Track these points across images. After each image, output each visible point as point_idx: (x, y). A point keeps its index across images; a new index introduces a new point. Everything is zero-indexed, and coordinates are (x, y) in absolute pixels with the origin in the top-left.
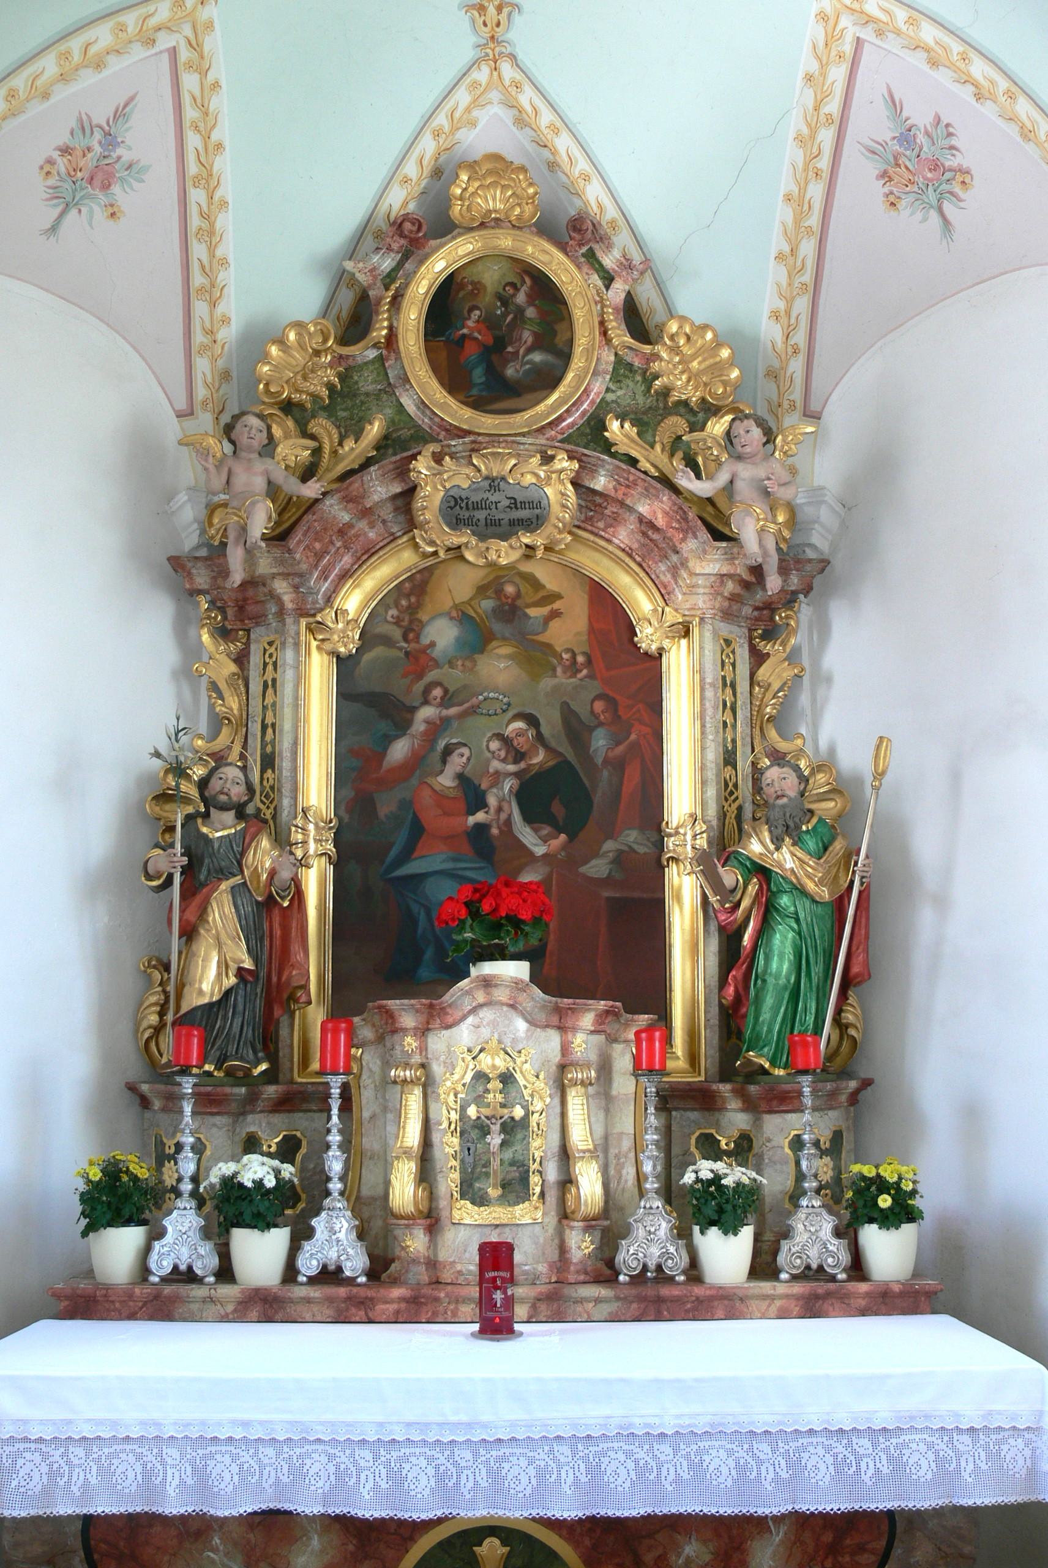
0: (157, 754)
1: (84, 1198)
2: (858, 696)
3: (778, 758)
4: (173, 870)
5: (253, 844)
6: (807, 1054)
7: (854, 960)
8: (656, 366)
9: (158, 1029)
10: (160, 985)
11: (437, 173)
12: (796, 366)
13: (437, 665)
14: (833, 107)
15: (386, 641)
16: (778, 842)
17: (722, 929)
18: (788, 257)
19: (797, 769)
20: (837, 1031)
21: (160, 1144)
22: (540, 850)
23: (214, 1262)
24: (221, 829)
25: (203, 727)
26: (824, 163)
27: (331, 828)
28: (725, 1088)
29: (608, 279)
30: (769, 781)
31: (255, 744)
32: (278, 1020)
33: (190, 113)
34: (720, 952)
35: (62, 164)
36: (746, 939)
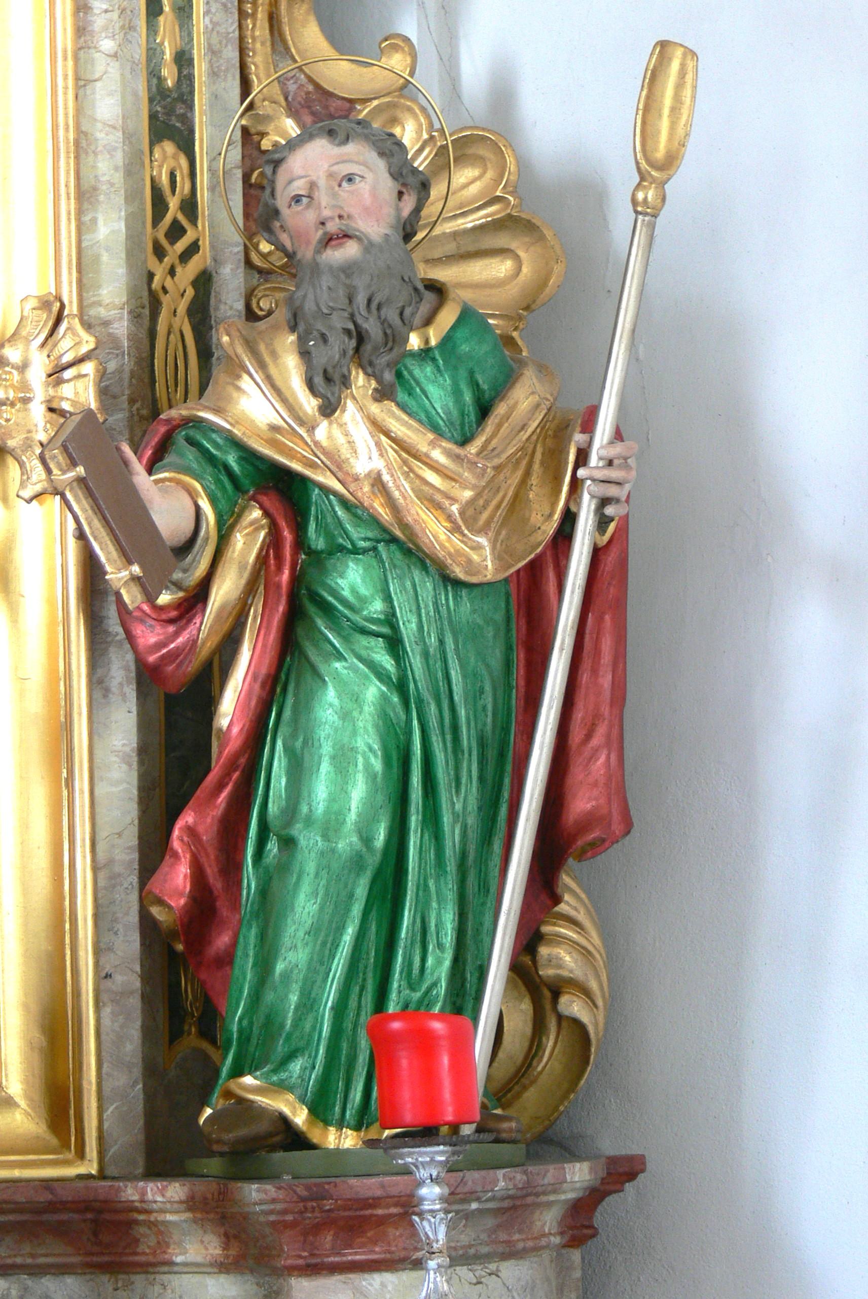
3: (327, 113)
6: (429, 1076)
7: (577, 774)
16: (329, 388)
17: (148, 676)
19: (390, 148)
20: (526, 1005)
28: (165, 1196)
30: (299, 187)
34: (143, 750)
36: (230, 707)
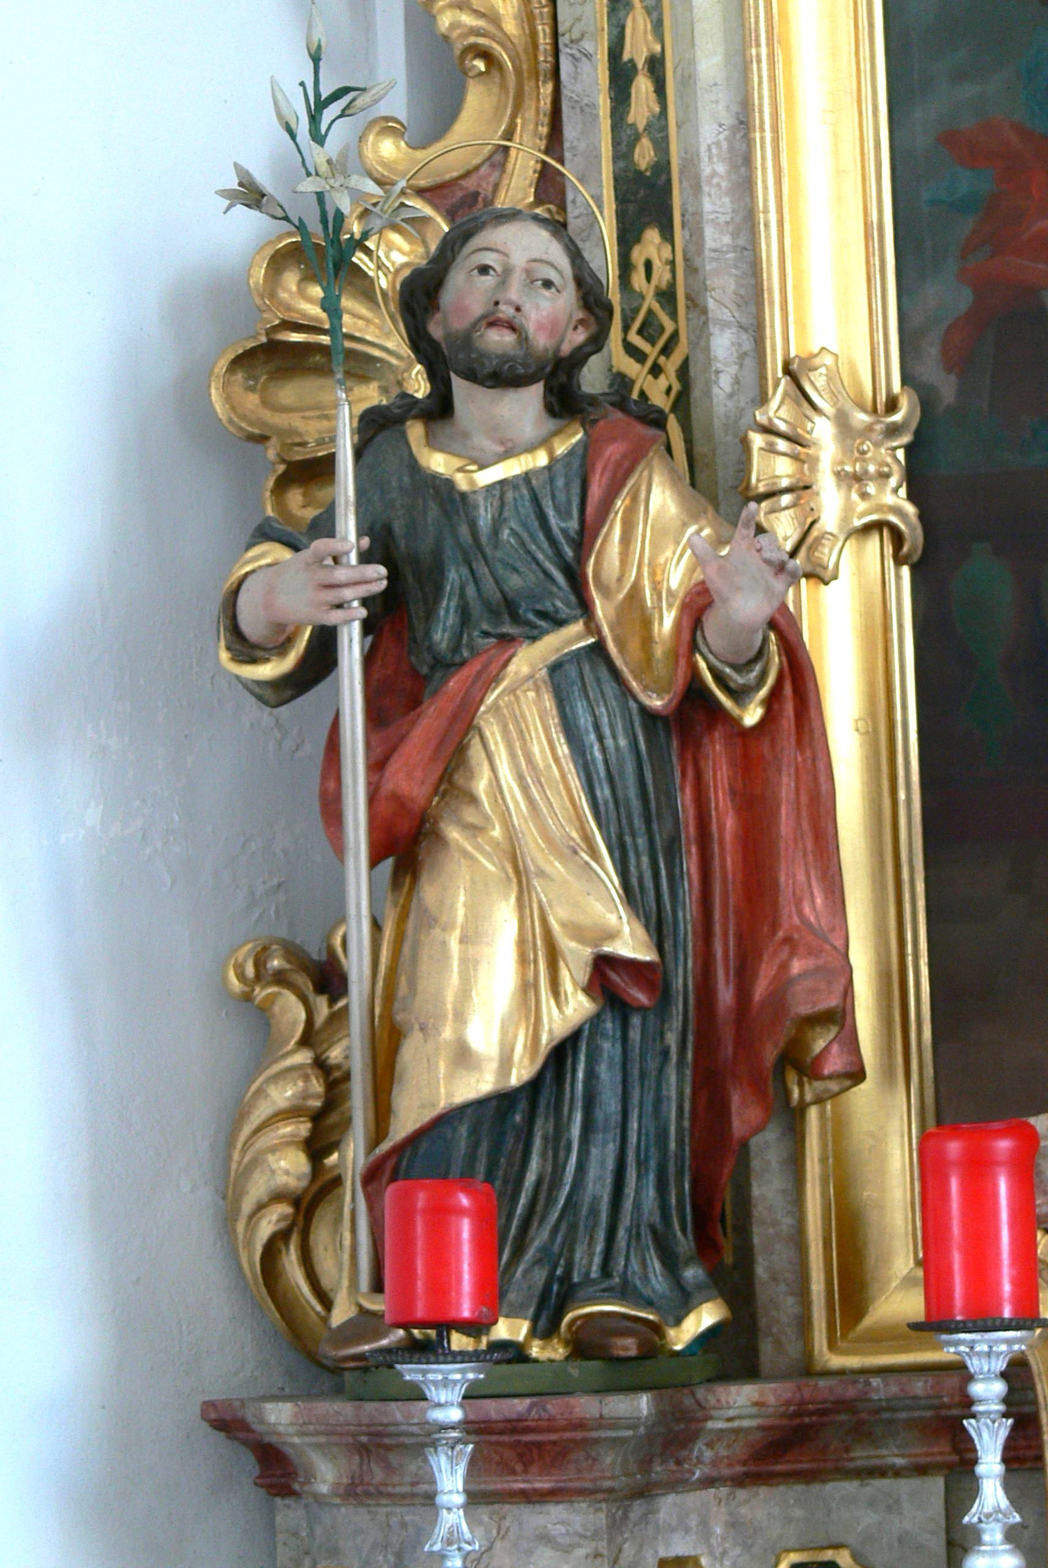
0: (251, 194)
4: (334, 617)
5: (620, 504)
9: (309, 1203)
10: (307, 1040)
24: (500, 451)
27: (893, 431)
31: (592, 140)
32: (744, 1144)
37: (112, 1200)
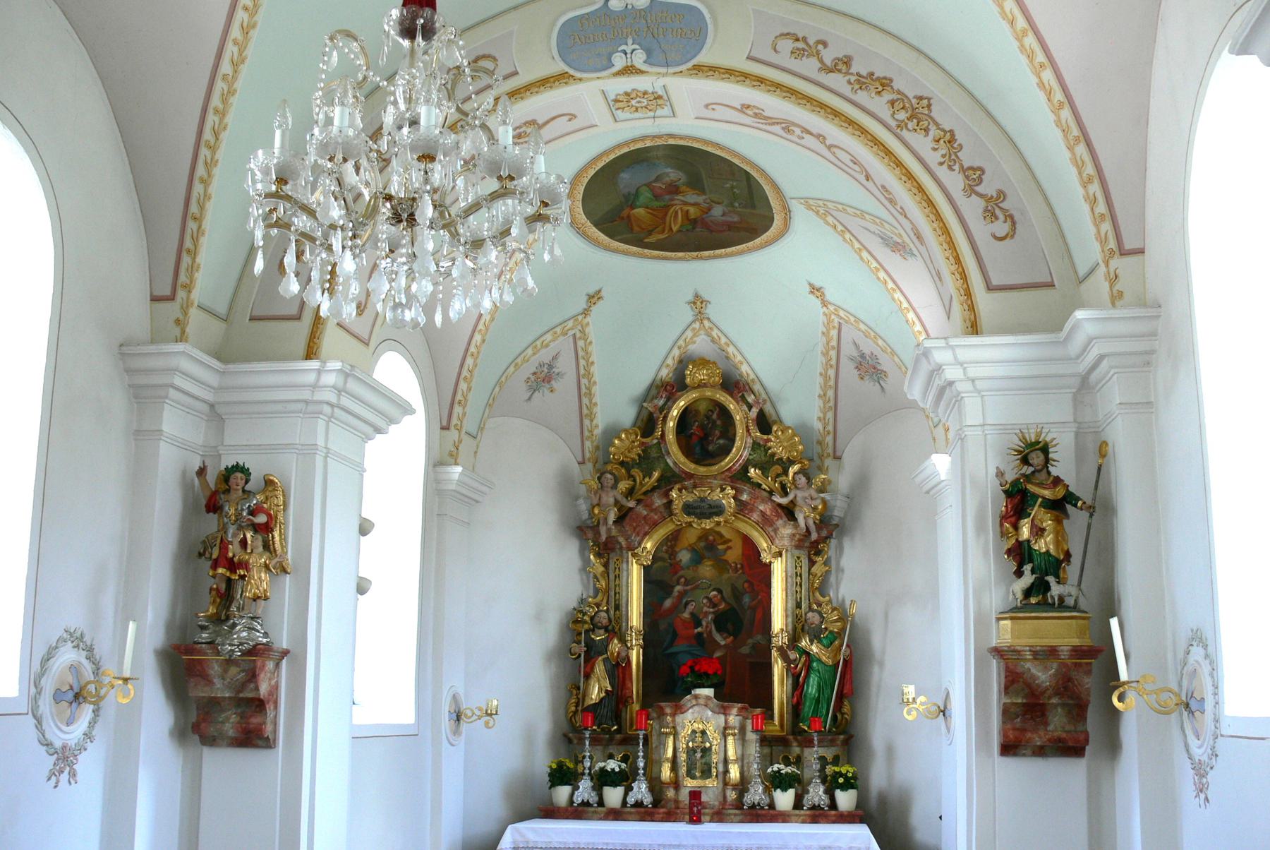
1: (550, 775)
2: (855, 577)
8: (769, 444)
9: (575, 713)
11: (681, 361)
12: (829, 439)
13: (682, 569)
14: (834, 343)
15: (662, 559)
18: (823, 396)
21: (576, 757)
22: (723, 643)
23: (596, 799)
24: (599, 637)
25: (591, 593)
26: (834, 362)
29: (750, 407)
33: (581, 353)
35: (533, 378)
37: (554, 712)
